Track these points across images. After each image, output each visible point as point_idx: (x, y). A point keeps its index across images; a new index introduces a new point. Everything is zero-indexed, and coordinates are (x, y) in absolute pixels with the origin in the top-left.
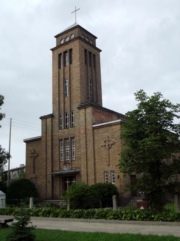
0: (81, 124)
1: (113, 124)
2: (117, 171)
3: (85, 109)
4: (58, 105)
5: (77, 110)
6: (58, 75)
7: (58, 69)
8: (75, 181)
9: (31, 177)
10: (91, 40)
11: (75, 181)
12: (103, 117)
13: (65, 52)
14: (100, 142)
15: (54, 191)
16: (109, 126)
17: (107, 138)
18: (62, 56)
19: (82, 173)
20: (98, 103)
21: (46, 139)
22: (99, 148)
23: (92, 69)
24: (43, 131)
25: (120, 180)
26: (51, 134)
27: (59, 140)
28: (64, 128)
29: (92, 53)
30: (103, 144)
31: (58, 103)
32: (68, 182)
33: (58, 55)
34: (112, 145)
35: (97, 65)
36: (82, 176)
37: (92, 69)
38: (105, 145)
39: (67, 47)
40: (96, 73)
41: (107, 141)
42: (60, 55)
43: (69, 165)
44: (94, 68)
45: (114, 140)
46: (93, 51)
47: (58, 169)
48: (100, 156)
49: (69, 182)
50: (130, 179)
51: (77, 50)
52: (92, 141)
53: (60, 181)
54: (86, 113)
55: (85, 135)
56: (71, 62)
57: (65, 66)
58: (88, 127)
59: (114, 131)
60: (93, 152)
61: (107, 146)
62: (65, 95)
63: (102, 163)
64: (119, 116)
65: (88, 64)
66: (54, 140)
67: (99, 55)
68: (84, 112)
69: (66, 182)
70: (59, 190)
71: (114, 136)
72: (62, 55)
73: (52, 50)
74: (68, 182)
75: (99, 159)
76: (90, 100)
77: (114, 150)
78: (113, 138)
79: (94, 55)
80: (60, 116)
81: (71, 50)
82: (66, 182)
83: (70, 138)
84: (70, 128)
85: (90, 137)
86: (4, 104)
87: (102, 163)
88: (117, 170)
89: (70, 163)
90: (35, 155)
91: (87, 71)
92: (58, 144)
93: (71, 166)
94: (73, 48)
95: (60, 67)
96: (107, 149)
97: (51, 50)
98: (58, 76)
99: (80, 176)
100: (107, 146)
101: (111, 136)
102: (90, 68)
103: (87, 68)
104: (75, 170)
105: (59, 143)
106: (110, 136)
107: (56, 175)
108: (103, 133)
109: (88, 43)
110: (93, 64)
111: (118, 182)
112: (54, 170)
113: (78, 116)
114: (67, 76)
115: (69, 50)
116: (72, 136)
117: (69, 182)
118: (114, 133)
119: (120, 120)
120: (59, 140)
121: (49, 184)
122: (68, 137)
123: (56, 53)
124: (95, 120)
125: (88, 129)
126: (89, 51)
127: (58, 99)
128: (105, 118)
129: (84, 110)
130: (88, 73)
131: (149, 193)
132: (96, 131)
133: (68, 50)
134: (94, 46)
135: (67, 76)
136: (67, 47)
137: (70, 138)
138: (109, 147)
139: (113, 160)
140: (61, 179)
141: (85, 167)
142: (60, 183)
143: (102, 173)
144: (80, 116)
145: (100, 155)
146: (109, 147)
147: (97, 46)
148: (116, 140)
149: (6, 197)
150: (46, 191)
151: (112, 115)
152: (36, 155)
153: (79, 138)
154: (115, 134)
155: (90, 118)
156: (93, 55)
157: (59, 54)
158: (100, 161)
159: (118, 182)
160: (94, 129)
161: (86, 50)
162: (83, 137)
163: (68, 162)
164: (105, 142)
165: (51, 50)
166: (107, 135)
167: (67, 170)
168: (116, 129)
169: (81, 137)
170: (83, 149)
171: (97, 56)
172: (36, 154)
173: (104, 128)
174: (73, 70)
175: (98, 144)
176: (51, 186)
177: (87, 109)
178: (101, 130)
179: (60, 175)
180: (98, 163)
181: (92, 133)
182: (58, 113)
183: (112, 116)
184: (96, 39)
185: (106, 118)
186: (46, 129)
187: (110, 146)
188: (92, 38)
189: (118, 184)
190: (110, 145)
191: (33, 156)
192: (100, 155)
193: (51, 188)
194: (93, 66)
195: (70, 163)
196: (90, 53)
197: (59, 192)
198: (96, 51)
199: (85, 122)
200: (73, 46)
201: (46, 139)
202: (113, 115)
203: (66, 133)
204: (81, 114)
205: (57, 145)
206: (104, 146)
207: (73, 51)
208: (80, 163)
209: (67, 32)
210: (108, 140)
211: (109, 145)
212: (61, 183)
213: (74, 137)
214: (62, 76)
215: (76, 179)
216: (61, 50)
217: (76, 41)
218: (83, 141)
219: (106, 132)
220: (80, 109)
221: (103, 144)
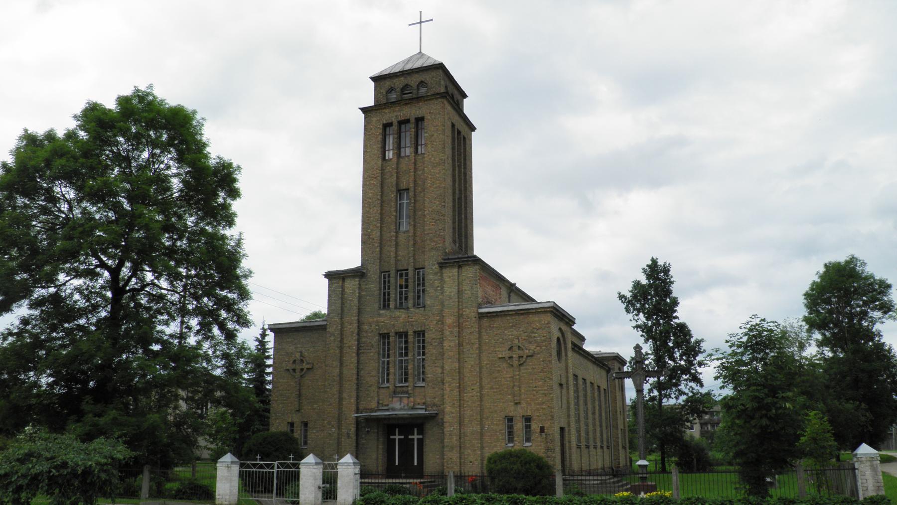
1: (534, 311)
2: (538, 416)
9: (290, 421)
14: (497, 349)
24: (333, 307)
25: (546, 438)
32: (397, 437)
48: (494, 380)
59: (534, 327)
71: (534, 337)
73: (365, 110)
74: (397, 437)
75: (494, 389)
77: (533, 369)
84: (412, 310)
88: (538, 414)
94: (428, 117)
97: (361, 109)
101: (526, 338)
118: (535, 331)
122: (405, 330)
123: (374, 119)
137: (410, 333)
138: (522, 362)
141: (454, 404)
143: (499, 420)
145: (496, 378)
154: (535, 333)
164: (294, 362)
167: (401, 409)
173: (508, 318)
180: (488, 395)
186: (343, 304)
219: (512, 326)
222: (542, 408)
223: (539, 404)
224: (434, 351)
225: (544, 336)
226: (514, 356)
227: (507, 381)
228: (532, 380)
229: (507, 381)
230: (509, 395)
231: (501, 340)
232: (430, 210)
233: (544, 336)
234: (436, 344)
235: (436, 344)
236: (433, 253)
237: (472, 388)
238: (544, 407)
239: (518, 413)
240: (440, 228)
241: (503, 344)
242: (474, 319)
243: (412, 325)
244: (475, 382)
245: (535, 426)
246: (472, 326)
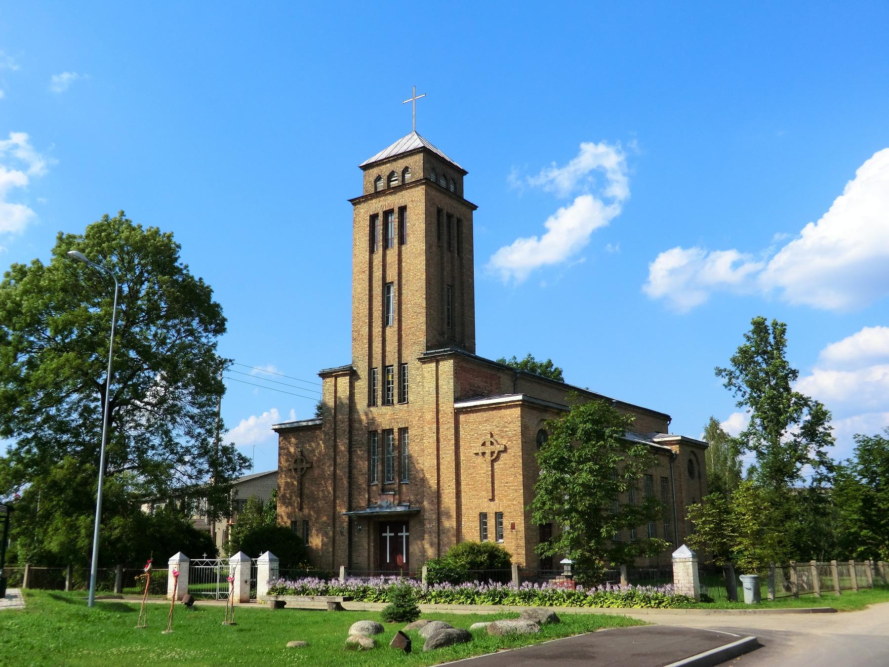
0: (426, 398)
2: (509, 512)
3: (437, 362)
4: (367, 346)
5: (419, 364)
6: (368, 269)
7: (368, 254)
8: (408, 534)
10: (453, 180)
11: (408, 534)
12: (479, 382)
13: (388, 213)
15: (354, 555)
16: (495, 409)
17: (489, 436)
18: (379, 222)
19: (427, 515)
20: (466, 344)
21: (335, 429)
22: (469, 459)
23: (453, 258)
25: (517, 535)
26: (347, 416)
27: (368, 432)
28: (383, 404)
29: (453, 215)
30: (480, 450)
31: (366, 341)
32: (388, 535)
33: (368, 218)
34: (502, 455)
35: (465, 245)
36: (426, 522)
37: (453, 258)
38: (484, 454)
39: (393, 201)
40: (461, 266)
41: (488, 444)
42: (373, 218)
43: (394, 495)
44: (458, 254)
45: (506, 441)
46: (457, 210)
47: (363, 504)
48: (470, 476)
49: (393, 534)
50: (539, 531)
51: (420, 213)
52: (453, 442)
53: (369, 531)
54: (440, 372)
55: (435, 426)
56: (402, 241)
57: (386, 247)
58: (442, 407)
60: (454, 466)
61: (487, 455)
62: (385, 323)
63: (474, 493)
64: (516, 376)
65: (445, 245)
66: (355, 432)
67: (471, 220)
68: (434, 368)
69: (384, 535)
70: (366, 554)
71: (506, 432)
72: (381, 218)
74: (388, 535)
76: (446, 336)
77: (505, 464)
78: (502, 437)
79: (459, 221)
80: (371, 371)
81: (403, 210)
82: (384, 535)
83: (396, 430)
84: (397, 406)
85: (448, 431)
86: (225, 334)
87: (474, 493)
88: (509, 510)
89: (397, 489)
90: (305, 465)
91: (442, 264)
92: (365, 442)
93: (397, 497)
94: (409, 205)
95: (372, 251)
96: (487, 461)
97: (350, 201)
98: (367, 272)
99: (422, 523)
100: (488, 455)
101: (498, 432)
102: (449, 254)
103: (442, 258)
104: (409, 506)
105: (369, 439)
106: (496, 431)
107: (361, 518)
108: (480, 423)
109: (446, 191)
110: (456, 245)
111: (512, 538)
112: (354, 505)
113: (419, 379)
114: (392, 275)
115: (399, 208)
116: (403, 426)
117: (393, 534)
118: (507, 425)
119: (520, 397)
120: (368, 432)
121: (342, 538)
122: (391, 428)
123: (362, 211)
124: (460, 389)
125: (442, 412)
126: (447, 212)
127: (367, 330)
128: (482, 384)
129: (434, 364)
130: (442, 269)
131: (29, 469)
132: (462, 418)
133: (396, 210)
134: (458, 195)
135: (392, 275)
136: (393, 201)
137: (396, 430)
138: (494, 457)
139: (501, 489)
140: (372, 527)
141: (433, 501)
142: (369, 537)
143: (474, 517)
144: (423, 377)
145: (471, 474)
146: (492, 456)
147: (468, 196)
148: (509, 443)
149: (279, 565)
150: (334, 555)
151: (499, 375)
152: (308, 465)
153: (420, 430)
155: (448, 385)
156: (456, 221)
157: (371, 216)
158: (470, 489)
159: (512, 538)
160: (458, 412)
161: (439, 211)
162: (430, 429)
163: (392, 486)
164: (484, 444)
165: (350, 201)
166: (489, 428)
168: (510, 415)
169: (426, 429)
170: (429, 457)
171: (465, 223)
172: (307, 463)
174: (408, 261)
175: (467, 449)
176: (347, 542)
177: (441, 363)
178: (473, 417)
179: (369, 518)
181: (452, 420)
182: (367, 364)
183: (500, 378)
184: (465, 177)
185: (486, 382)
187: (495, 455)
188: (456, 176)
189: (511, 542)
190: (496, 452)
191: (300, 467)
192: (471, 474)
193: (346, 547)
194: (456, 249)
195: (397, 489)
196: (450, 216)
197: (366, 560)
198: (463, 209)
199: (437, 393)
200: (410, 200)
201: (335, 429)
202: (502, 376)
203: (388, 417)
204: (426, 375)
205: (363, 444)
206: (480, 454)
207: (408, 213)
208: (421, 490)
209: (395, 160)
210: (491, 442)
211: (492, 453)
212: (372, 537)
213: (408, 428)
214: (378, 274)
215: (410, 528)
216: (378, 205)
217: (417, 189)
218: (431, 440)
220: (424, 363)
221: (477, 448)
222: (513, 505)
223: (510, 500)
224: (417, 448)
225: (515, 431)
226: (487, 451)
227: (482, 477)
228: (503, 475)
229: (482, 477)
230: (483, 491)
231: (476, 435)
232: (413, 303)
233: (515, 431)
234: (418, 440)
235: (418, 440)
236: (416, 347)
237: (449, 484)
238: (514, 503)
239: (491, 509)
240: (421, 321)
241: (478, 439)
242: (450, 414)
243: (397, 422)
244: (451, 478)
245: (506, 523)
246: (449, 422)
